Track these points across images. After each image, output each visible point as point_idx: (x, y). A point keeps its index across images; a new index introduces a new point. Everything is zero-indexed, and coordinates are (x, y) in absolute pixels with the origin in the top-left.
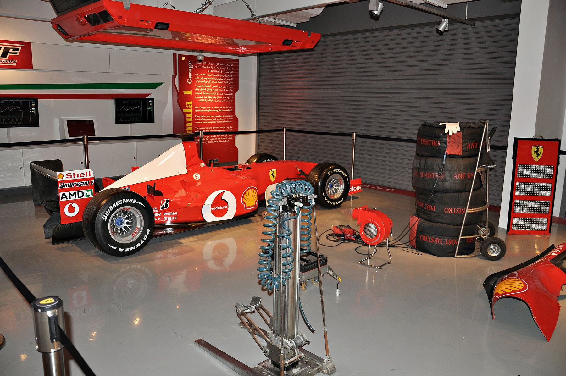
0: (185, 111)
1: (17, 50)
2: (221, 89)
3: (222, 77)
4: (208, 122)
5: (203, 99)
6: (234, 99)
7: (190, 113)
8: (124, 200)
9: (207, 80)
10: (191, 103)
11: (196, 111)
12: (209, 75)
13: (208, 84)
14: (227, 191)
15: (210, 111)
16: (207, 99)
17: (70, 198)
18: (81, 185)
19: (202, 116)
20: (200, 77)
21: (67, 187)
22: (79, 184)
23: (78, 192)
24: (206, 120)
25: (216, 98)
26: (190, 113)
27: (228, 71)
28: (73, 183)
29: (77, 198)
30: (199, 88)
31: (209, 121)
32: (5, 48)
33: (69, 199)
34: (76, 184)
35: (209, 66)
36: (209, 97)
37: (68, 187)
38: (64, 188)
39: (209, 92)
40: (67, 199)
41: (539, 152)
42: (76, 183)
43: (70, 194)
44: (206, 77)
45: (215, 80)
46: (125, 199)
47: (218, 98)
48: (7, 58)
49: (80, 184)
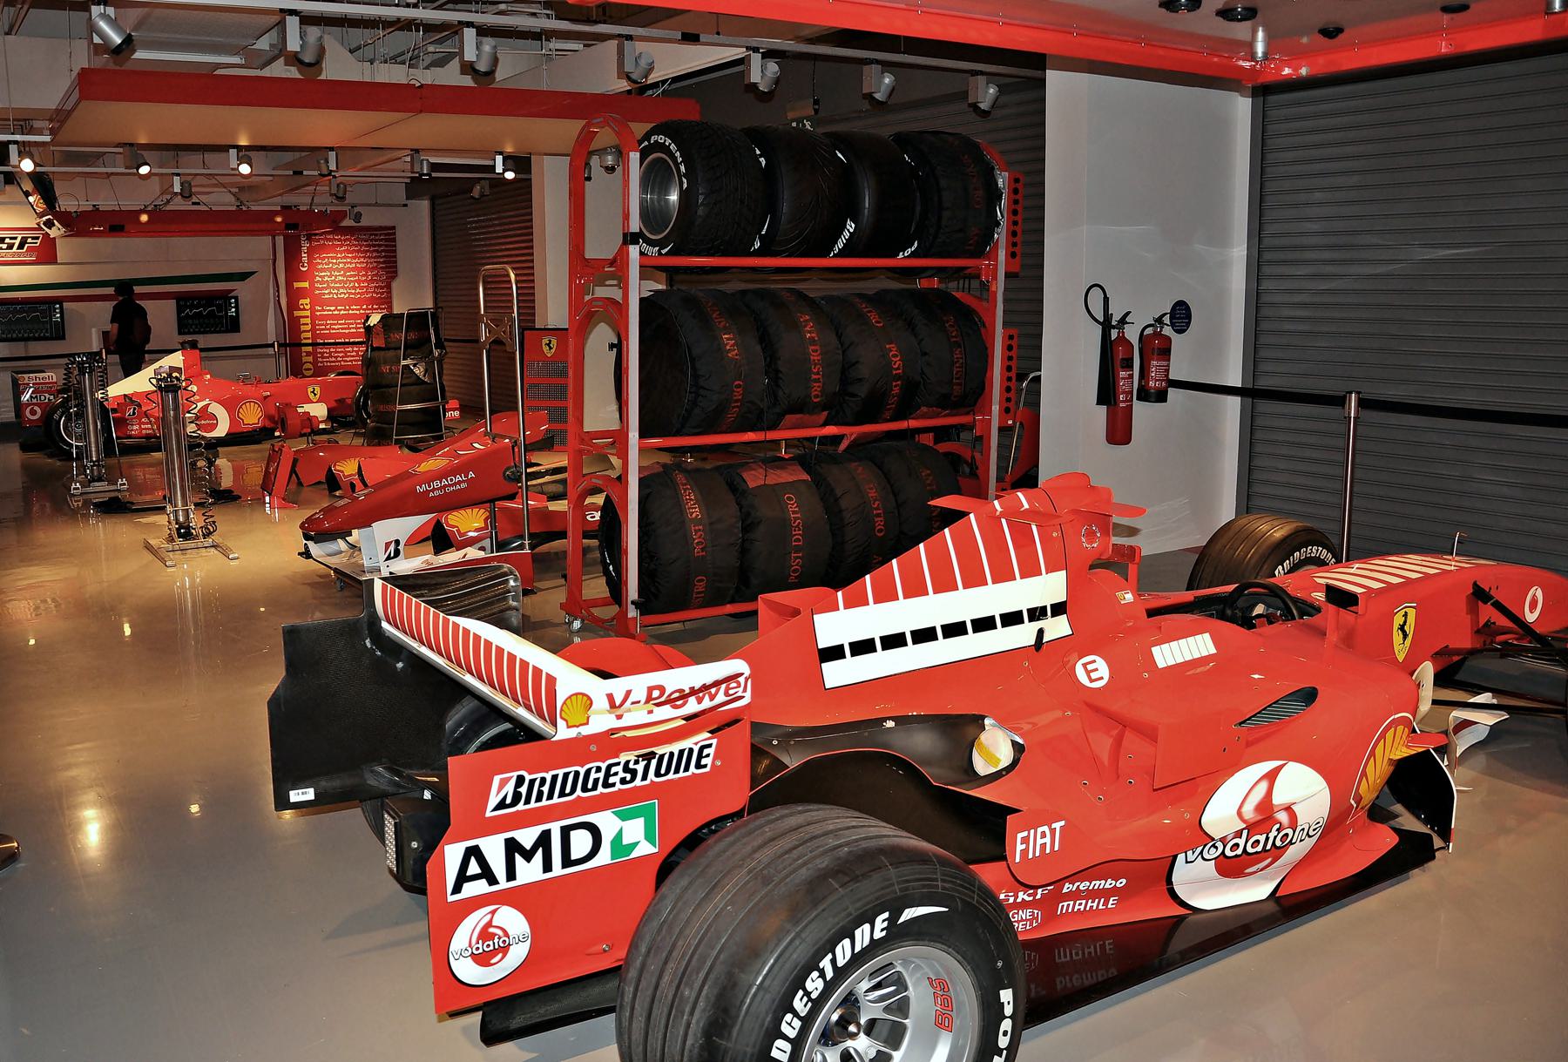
0: (297, 313)
1: (37, 238)
2: (363, 275)
3: (364, 257)
4: (341, 331)
5: (329, 293)
6: (390, 292)
7: (307, 317)
8: (826, 963)
9: (336, 264)
10: (308, 301)
11: (318, 313)
12: (339, 255)
13: (339, 271)
14: (1291, 763)
15: (342, 312)
16: (337, 294)
17: (511, 875)
18: (633, 779)
19: (328, 322)
20: (324, 258)
21: (539, 799)
22: (622, 775)
23: (566, 832)
24: (336, 327)
25: (353, 291)
26: (307, 317)
27: (374, 246)
28: (582, 771)
29: (558, 870)
30: (320, 277)
31: (342, 329)
32: (22, 238)
33: (503, 884)
34: (601, 775)
35: (339, 240)
36: (342, 291)
37: (550, 797)
38: (521, 807)
39: (340, 282)
40: (492, 880)
41: (551, 345)
42: (599, 769)
43: (512, 847)
44: (333, 258)
45: (351, 263)
46: (830, 956)
47: (358, 290)
48: (25, 250)
49: (626, 769)
